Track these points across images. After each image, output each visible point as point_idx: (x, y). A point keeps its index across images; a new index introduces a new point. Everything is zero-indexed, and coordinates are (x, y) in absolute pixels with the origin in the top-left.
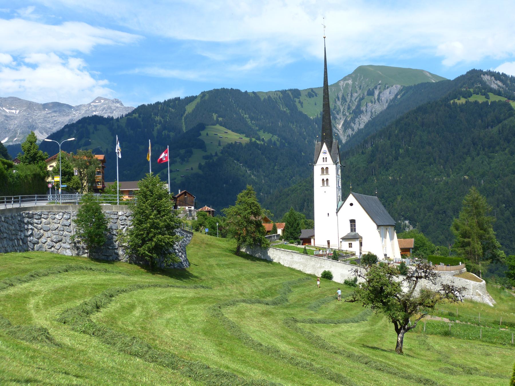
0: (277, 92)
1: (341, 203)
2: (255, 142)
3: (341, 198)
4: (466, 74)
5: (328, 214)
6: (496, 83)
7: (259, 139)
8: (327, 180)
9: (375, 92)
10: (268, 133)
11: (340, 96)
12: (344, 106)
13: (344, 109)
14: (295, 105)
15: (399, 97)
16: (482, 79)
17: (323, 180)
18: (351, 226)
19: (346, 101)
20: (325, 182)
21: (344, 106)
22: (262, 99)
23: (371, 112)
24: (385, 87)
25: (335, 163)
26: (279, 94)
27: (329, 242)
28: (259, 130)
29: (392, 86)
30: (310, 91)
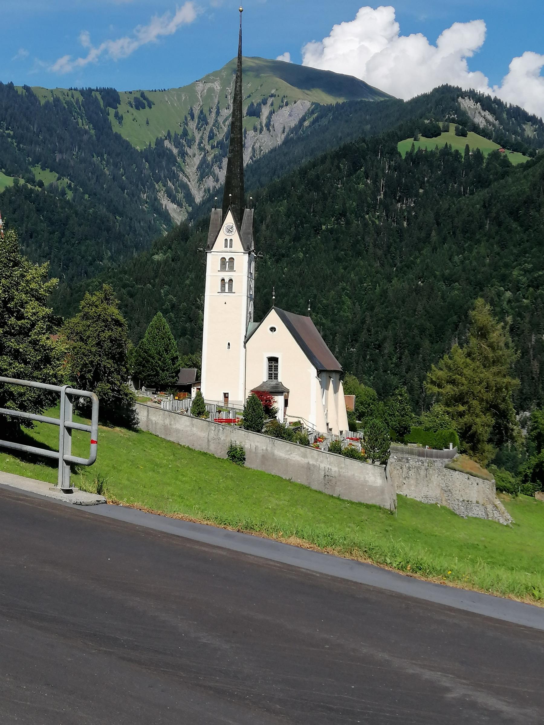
0: (73, 91)
1: (252, 325)
2: (25, 186)
3: (252, 315)
4: (432, 93)
5: (229, 344)
6: (483, 115)
7: (31, 180)
8: (231, 280)
9: (263, 110)
10: (51, 171)
11: (196, 113)
12: (201, 132)
13: (202, 138)
14: (106, 120)
15: (306, 123)
16: (459, 104)
17: (223, 280)
18: (270, 368)
19: (207, 124)
20: (227, 286)
21: (201, 132)
22: (43, 102)
23: (253, 148)
24: (283, 102)
25: (247, 250)
26: (77, 95)
27: (226, 396)
28: (33, 164)
29: (295, 103)
30: (138, 96)
